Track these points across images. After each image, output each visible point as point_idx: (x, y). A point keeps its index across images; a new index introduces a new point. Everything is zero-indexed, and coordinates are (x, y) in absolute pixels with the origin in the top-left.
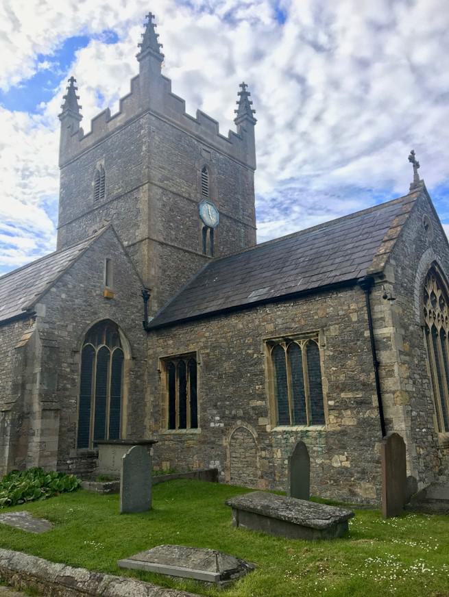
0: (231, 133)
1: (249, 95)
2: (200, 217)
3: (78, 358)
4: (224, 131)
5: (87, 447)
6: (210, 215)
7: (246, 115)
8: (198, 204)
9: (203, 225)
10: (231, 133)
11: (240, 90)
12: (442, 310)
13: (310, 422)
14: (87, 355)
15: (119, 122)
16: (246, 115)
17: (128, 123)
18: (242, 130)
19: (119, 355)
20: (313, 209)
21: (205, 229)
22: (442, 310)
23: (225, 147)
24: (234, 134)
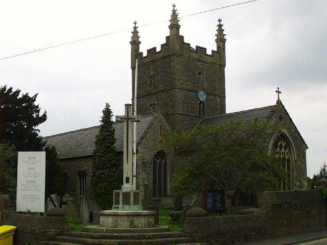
0: (213, 51)
1: (208, 68)
2: (198, 98)
3: (152, 166)
4: (209, 52)
5: (123, 204)
6: (202, 96)
7: (221, 40)
8: (196, 92)
9: (199, 102)
10: (213, 51)
11: (218, 23)
12: (285, 150)
13: (130, 193)
14: (155, 163)
15: (160, 55)
16: (221, 40)
17: (165, 57)
18: (218, 47)
19: (166, 163)
20: (124, 227)
21: (200, 104)
22: (285, 150)
23: (209, 60)
24: (215, 51)
